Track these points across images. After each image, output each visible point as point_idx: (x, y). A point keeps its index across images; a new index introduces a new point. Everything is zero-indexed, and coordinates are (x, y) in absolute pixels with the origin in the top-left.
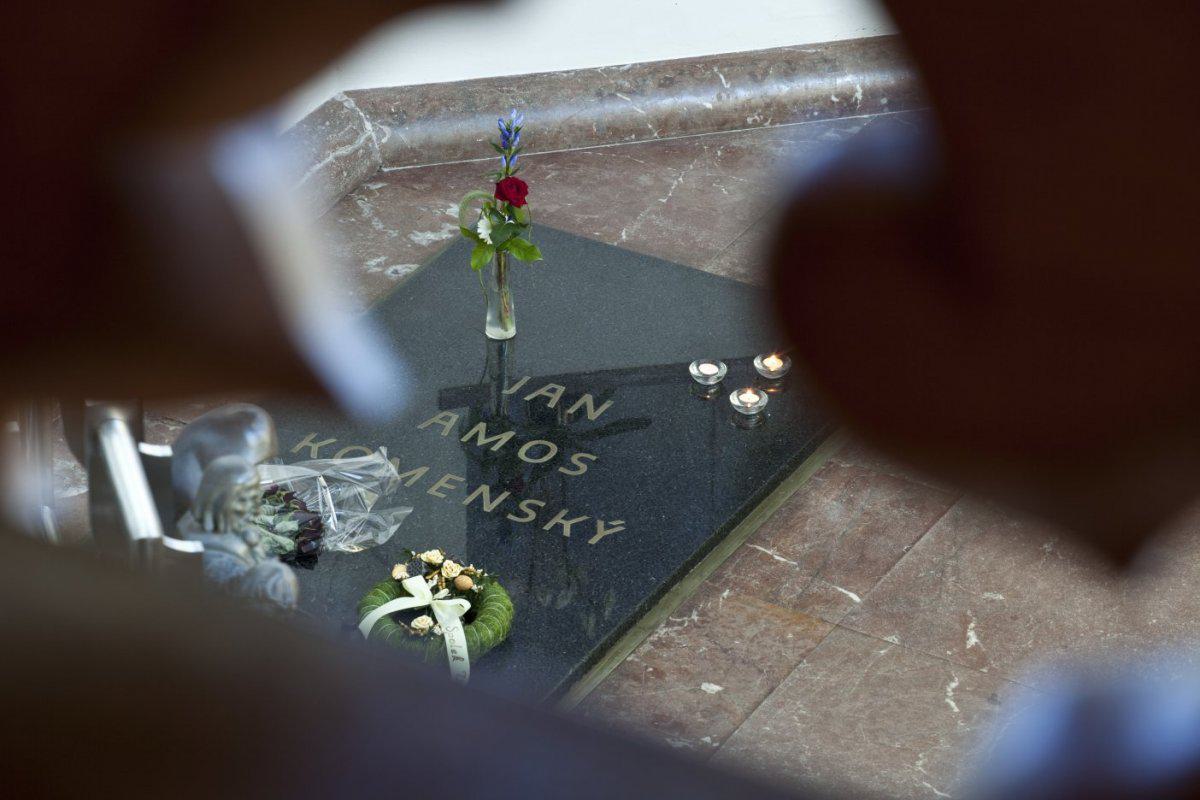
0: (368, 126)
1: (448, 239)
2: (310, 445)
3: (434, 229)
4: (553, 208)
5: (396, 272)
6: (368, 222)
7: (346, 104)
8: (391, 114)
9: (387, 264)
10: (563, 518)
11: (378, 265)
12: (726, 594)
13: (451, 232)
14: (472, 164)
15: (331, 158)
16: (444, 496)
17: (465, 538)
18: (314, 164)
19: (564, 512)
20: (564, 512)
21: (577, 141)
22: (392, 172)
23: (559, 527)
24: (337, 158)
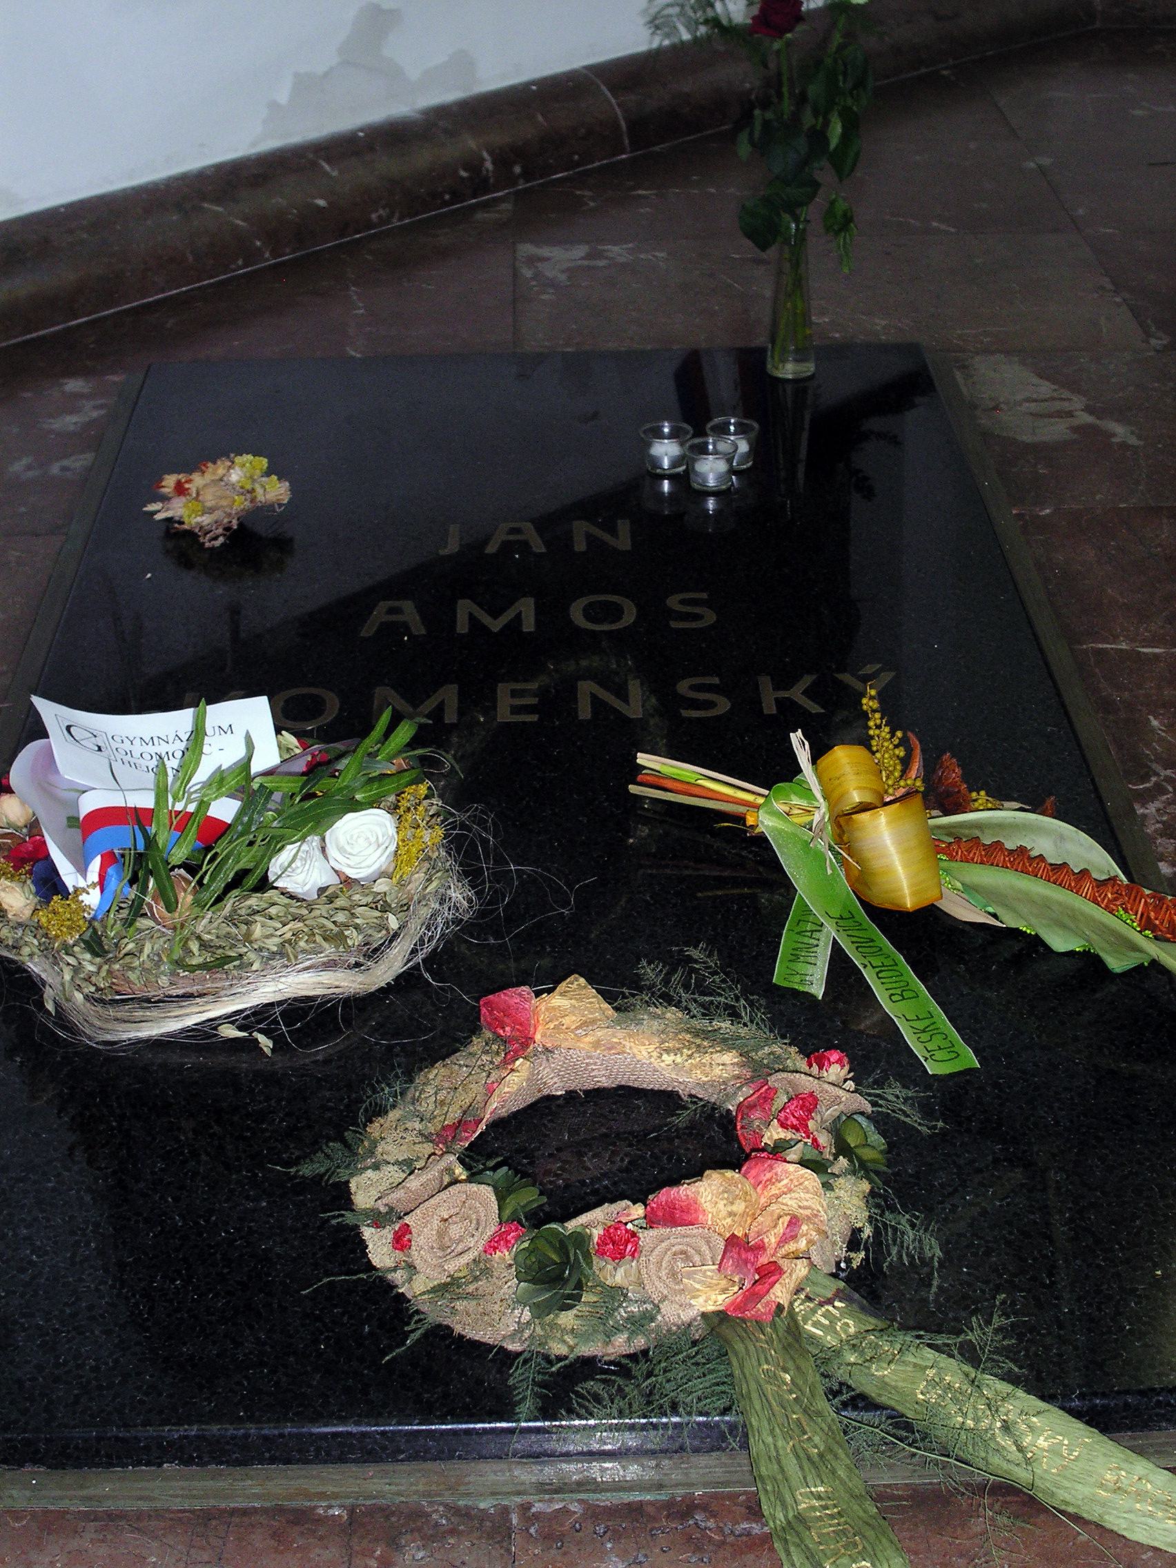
16: (534, 718)
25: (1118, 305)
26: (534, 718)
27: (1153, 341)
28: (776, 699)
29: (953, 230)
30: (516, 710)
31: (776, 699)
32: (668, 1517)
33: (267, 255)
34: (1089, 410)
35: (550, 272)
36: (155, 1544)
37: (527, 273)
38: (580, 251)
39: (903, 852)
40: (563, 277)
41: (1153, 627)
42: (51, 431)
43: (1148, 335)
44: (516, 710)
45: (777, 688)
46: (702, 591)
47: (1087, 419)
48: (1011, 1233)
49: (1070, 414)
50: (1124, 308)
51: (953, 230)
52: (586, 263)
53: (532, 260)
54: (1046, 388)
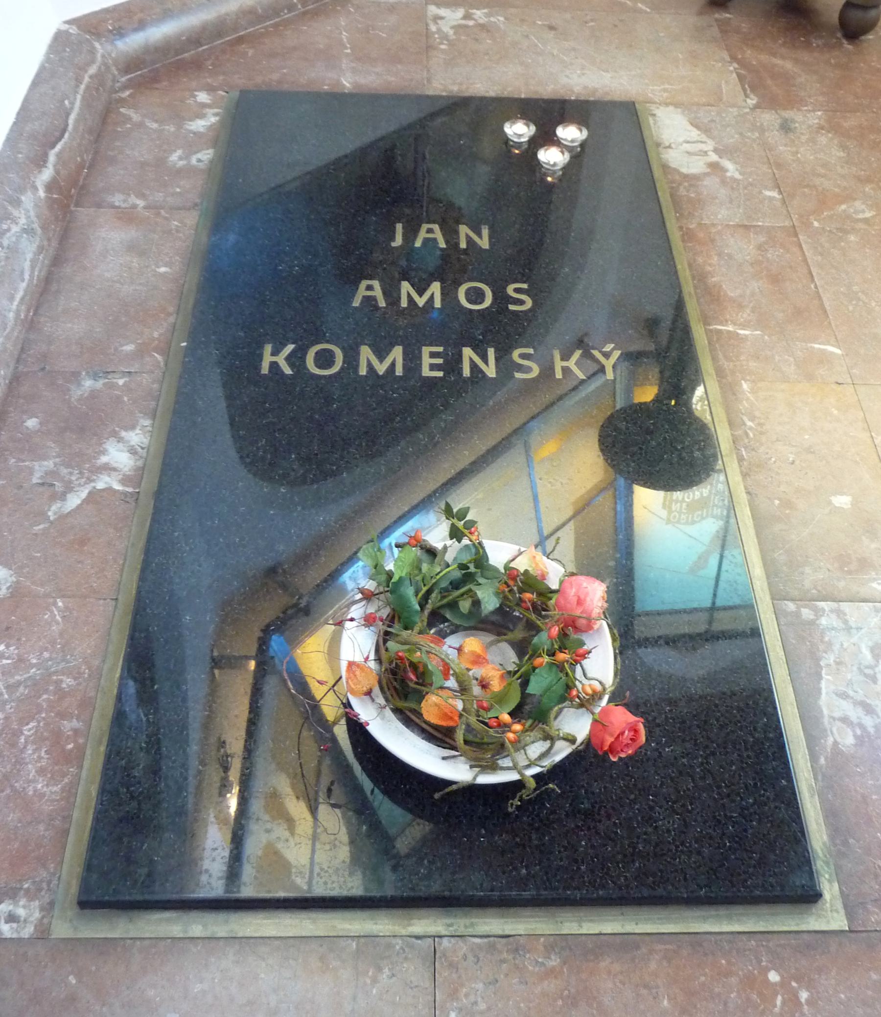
0: (97, 45)
1: (218, 121)
2: (274, 359)
3: (202, 116)
4: (275, 76)
5: (199, 161)
6: (141, 125)
7: (71, 31)
8: (111, 31)
9: (187, 157)
10: (273, 354)
11: (180, 158)
12: (745, 386)
13: (215, 115)
14: (184, 58)
15: (87, 79)
16: (440, 374)
17: (222, 400)
18: (77, 86)
19: (268, 348)
20: (268, 348)
21: (252, 24)
22: (129, 80)
23: (274, 366)
24: (91, 77)
25: (731, 72)
26: (440, 374)
27: (749, 101)
28: (562, 367)
29: (648, 10)
30: (433, 367)
31: (562, 367)
32: (507, 952)
33: (300, 7)
34: (715, 150)
35: (446, 29)
36: (264, 965)
37: (433, 28)
38: (460, 13)
39: (729, 918)
40: (451, 32)
41: (745, 316)
42: (191, 131)
43: (747, 96)
44: (433, 367)
45: (562, 359)
46: (524, 282)
47: (714, 157)
48: (673, 772)
49: (706, 153)
50: (734, 75)
51: (648, 10)
52: (463, 22)
53: (437, 18)
54: (695, 134)
